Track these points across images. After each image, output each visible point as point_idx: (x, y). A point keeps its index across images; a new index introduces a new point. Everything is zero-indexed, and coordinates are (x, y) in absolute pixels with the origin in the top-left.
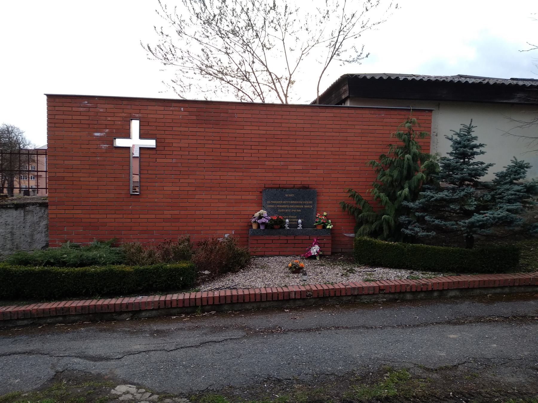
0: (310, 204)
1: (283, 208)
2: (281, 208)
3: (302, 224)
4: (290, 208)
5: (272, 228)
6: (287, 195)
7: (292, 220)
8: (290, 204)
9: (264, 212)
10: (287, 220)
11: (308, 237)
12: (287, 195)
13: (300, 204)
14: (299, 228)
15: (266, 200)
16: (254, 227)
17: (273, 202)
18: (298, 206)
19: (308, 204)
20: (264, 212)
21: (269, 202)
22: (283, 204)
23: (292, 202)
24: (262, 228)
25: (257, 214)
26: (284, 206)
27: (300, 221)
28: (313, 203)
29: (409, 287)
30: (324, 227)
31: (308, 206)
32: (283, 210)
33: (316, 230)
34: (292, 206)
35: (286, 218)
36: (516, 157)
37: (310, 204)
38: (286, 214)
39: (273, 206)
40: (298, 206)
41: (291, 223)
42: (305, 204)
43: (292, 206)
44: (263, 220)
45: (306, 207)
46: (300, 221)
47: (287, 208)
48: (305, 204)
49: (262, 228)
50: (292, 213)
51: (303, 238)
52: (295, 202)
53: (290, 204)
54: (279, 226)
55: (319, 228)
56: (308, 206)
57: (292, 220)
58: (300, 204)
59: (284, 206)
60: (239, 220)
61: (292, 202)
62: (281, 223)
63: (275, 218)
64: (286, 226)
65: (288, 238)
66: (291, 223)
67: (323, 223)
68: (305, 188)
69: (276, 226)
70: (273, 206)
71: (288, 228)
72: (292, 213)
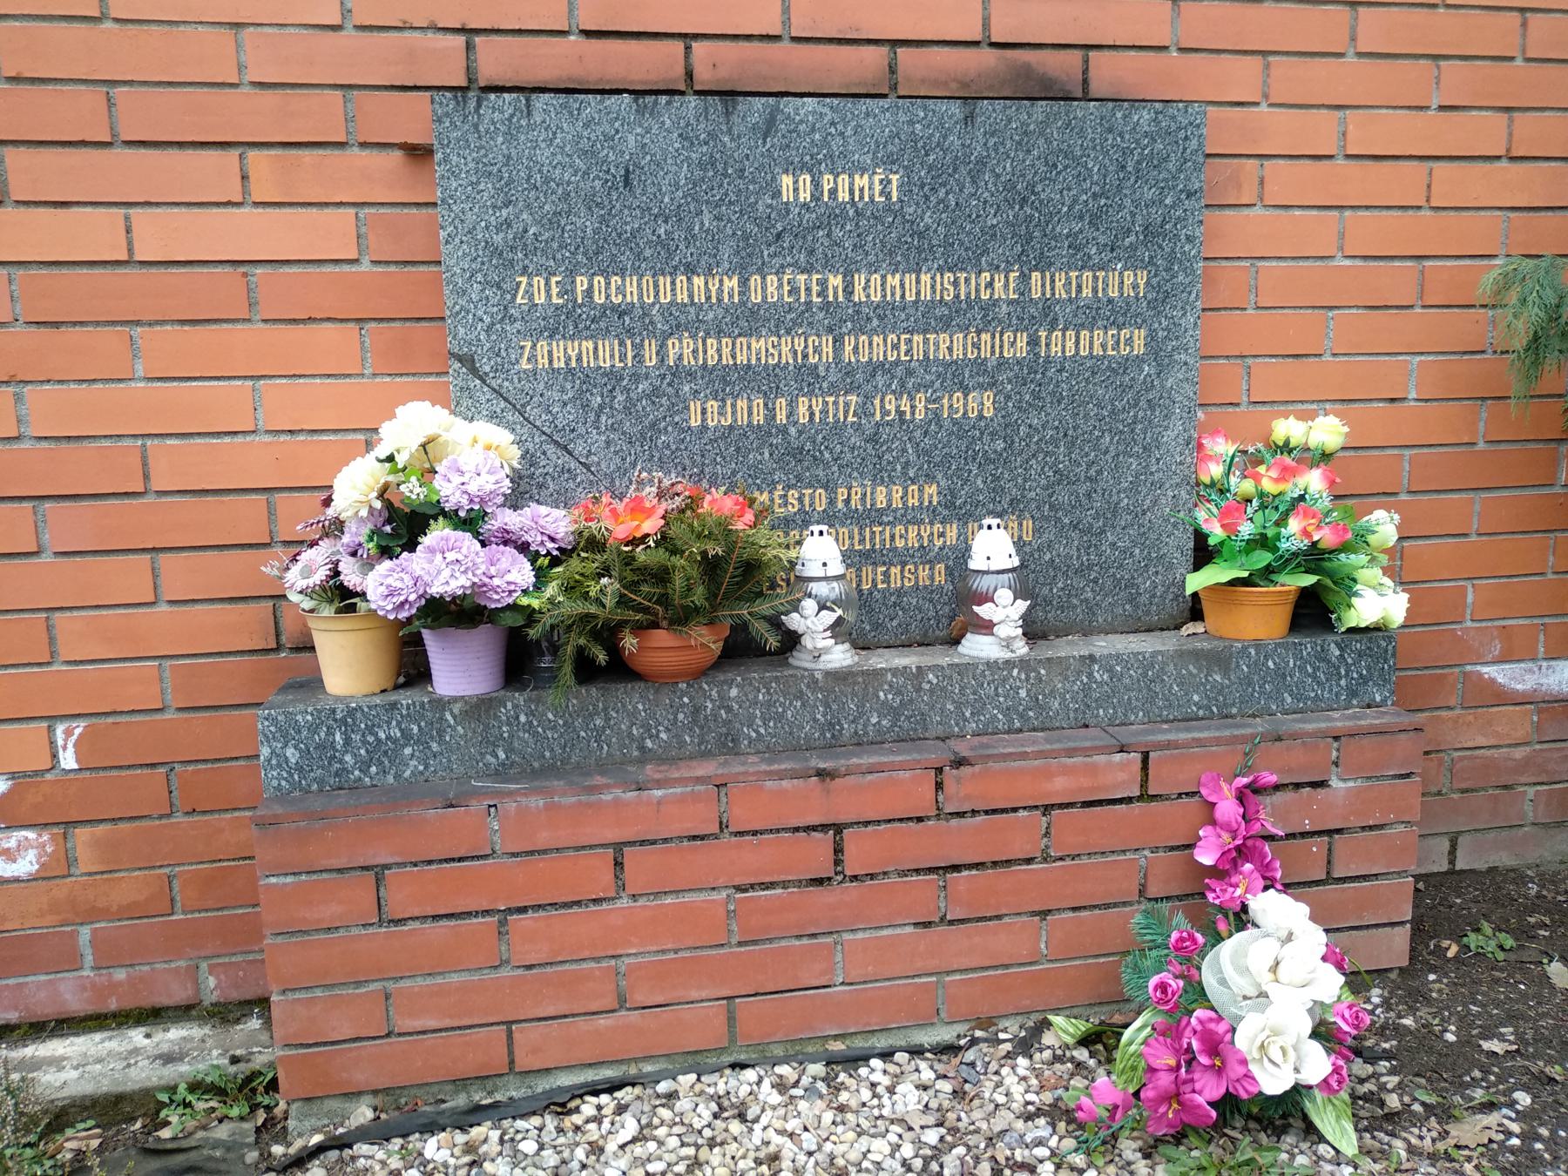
0: (1114, 314)
1: (764, 380)
2: (725, 381)
3: (1025, 581)
4: (850, 378)
5: (605, 667)
6: (794, 188)
7: (880, 535)
8: (844, 319)
9: (476, 454)
10: (821, 553)
11: (1120, 773)
12: (794, 188)
13: (985, 316)
14: (976, 647)
15: (505, 259)
16: (346, 665)
17: (603, 290)
18: (950, 346)
19: (1087, 318)
20: (476, 454)
21: (540, 291)
22: (748, 319)
23: (870, 287)
24: (459, 670)
25: (355, 488)
26: (759, 349)
27: (993, 548)
28: (1161, 297)
29: (1241, 1070)
30: (1313, 612)
31: (1097, 342)
32: (748, 410)
33: (1219, 659)
34: (878, 348)
35: (804, 520)
36: (1163, 54)
37: (1114, 314)
38: (801, 456)
39: (605, 354)
40: (950, 346)
41: (872, 576)
42: (1048, 314)
43: (878, 348)
44: (442, 565)
45: (1061, 344)
46: (993, 548)
47: (807, 377)
48: (1048, 314)
49: (459, 670)
50: (877, 453)
51: (1059, 787)
52: (924, 285)
53: (844, 319)
54: (707, 639)
55: (1260, 621)
56: (1097, 342)
57: (880, 535)
58: (985, 316)
59: (759, 349)
60: (130, 579)
61: (870, 287)
62: (723, 600)
63: (635, 515)
64: (812, 622)
65: (843, 803)
66: (872, 576)
67: (1314, 557)
68: (1038, 83)
69: (658, 648)
70: (605, 354)
71: (840, 656)
72: (877, 453)
